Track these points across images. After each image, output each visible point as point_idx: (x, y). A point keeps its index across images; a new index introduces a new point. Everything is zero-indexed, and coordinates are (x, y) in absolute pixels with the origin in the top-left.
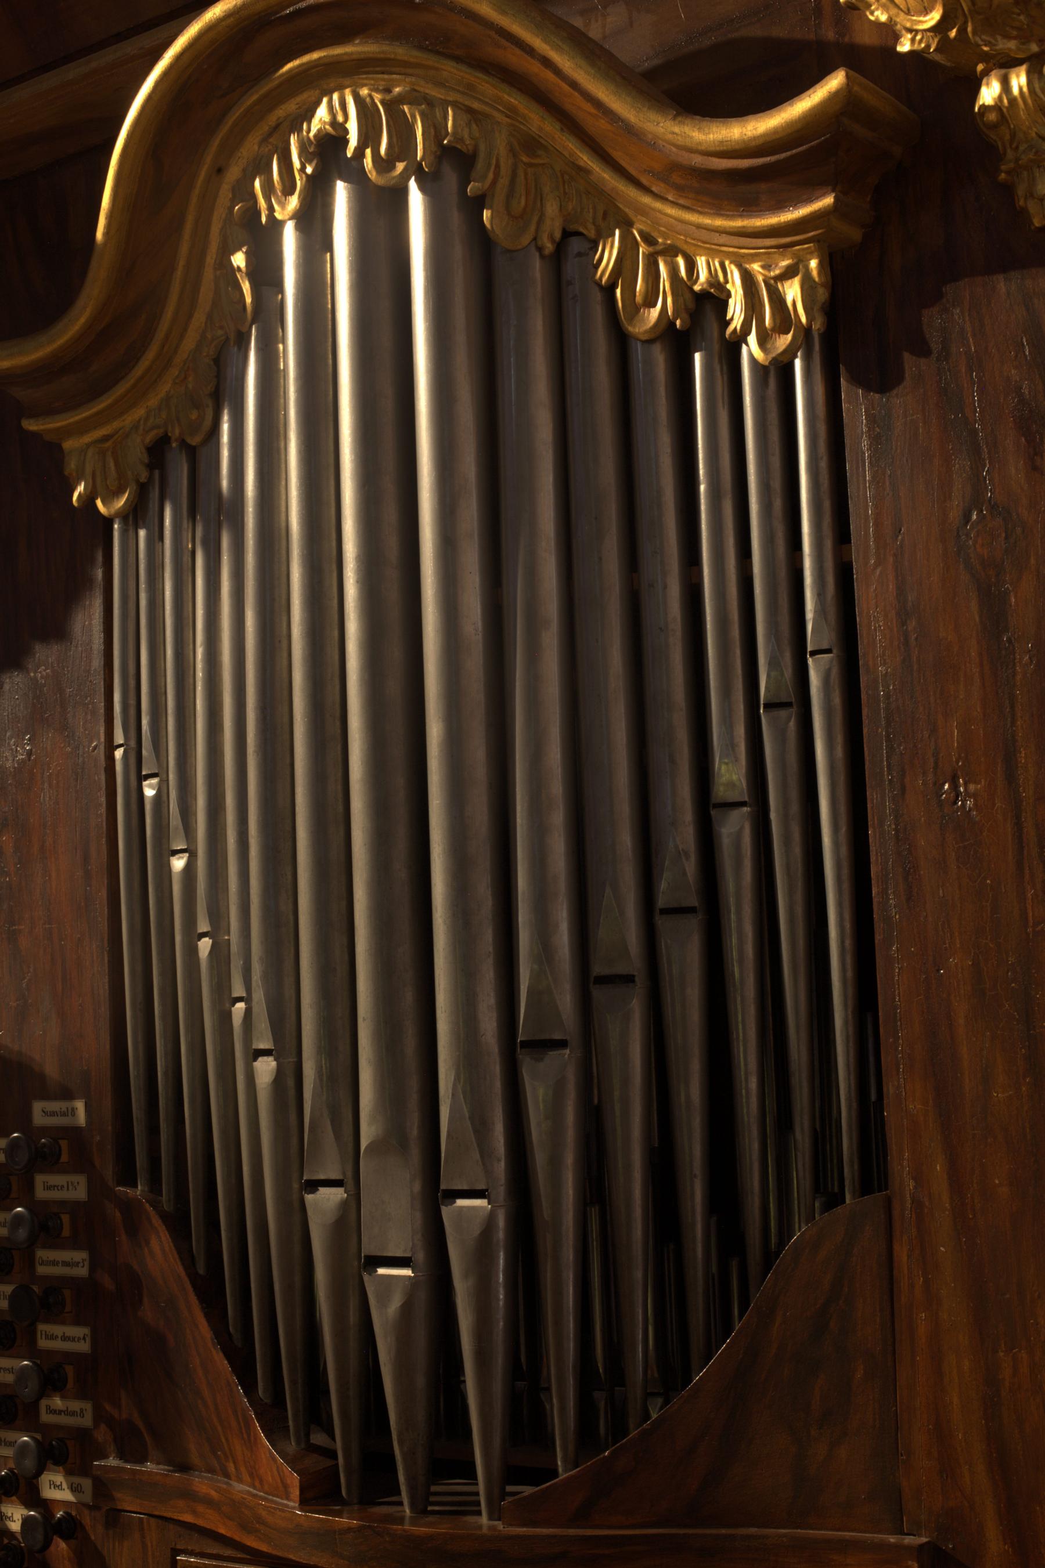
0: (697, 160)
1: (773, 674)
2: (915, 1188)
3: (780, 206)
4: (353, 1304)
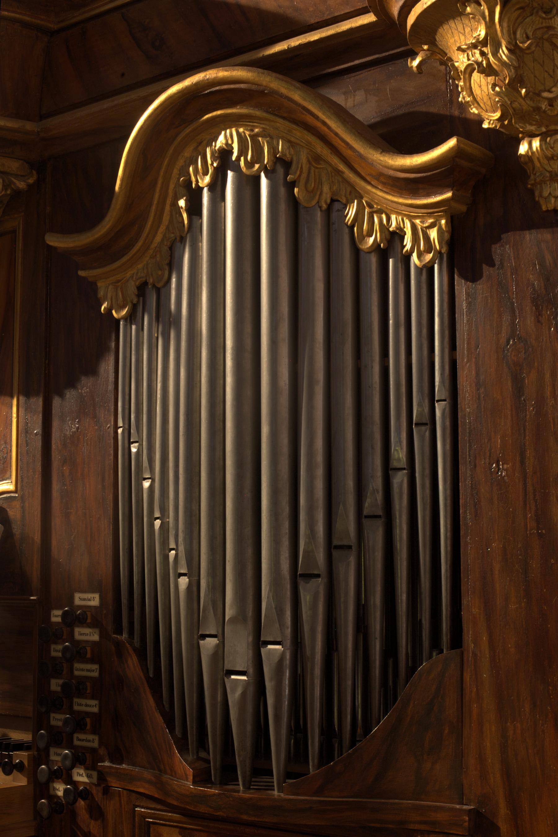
0: (391, 173)
1: (419, 409)
2: (474, 647)
3: (428, 195)
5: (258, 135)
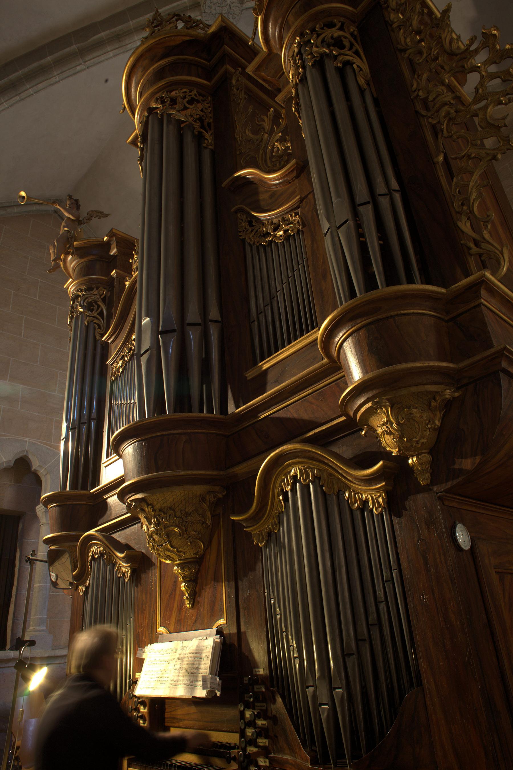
3: (376, 485)
4: (318, 714)
5: (307, 468)
